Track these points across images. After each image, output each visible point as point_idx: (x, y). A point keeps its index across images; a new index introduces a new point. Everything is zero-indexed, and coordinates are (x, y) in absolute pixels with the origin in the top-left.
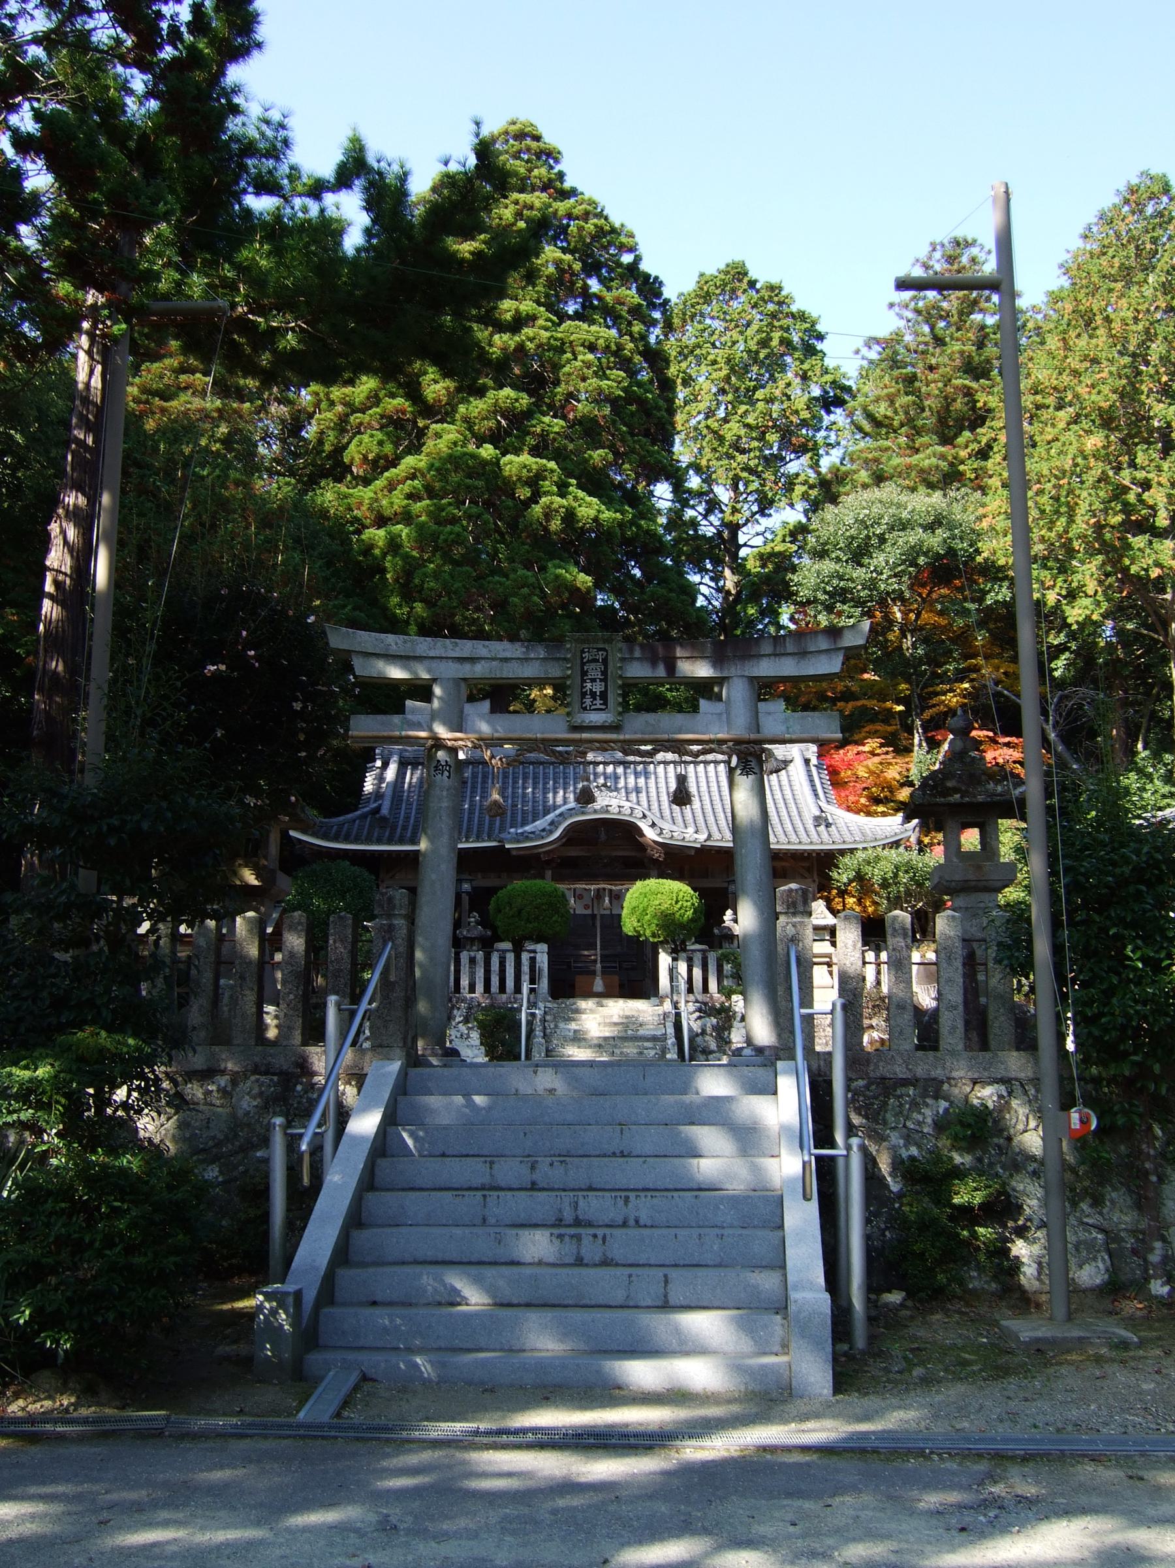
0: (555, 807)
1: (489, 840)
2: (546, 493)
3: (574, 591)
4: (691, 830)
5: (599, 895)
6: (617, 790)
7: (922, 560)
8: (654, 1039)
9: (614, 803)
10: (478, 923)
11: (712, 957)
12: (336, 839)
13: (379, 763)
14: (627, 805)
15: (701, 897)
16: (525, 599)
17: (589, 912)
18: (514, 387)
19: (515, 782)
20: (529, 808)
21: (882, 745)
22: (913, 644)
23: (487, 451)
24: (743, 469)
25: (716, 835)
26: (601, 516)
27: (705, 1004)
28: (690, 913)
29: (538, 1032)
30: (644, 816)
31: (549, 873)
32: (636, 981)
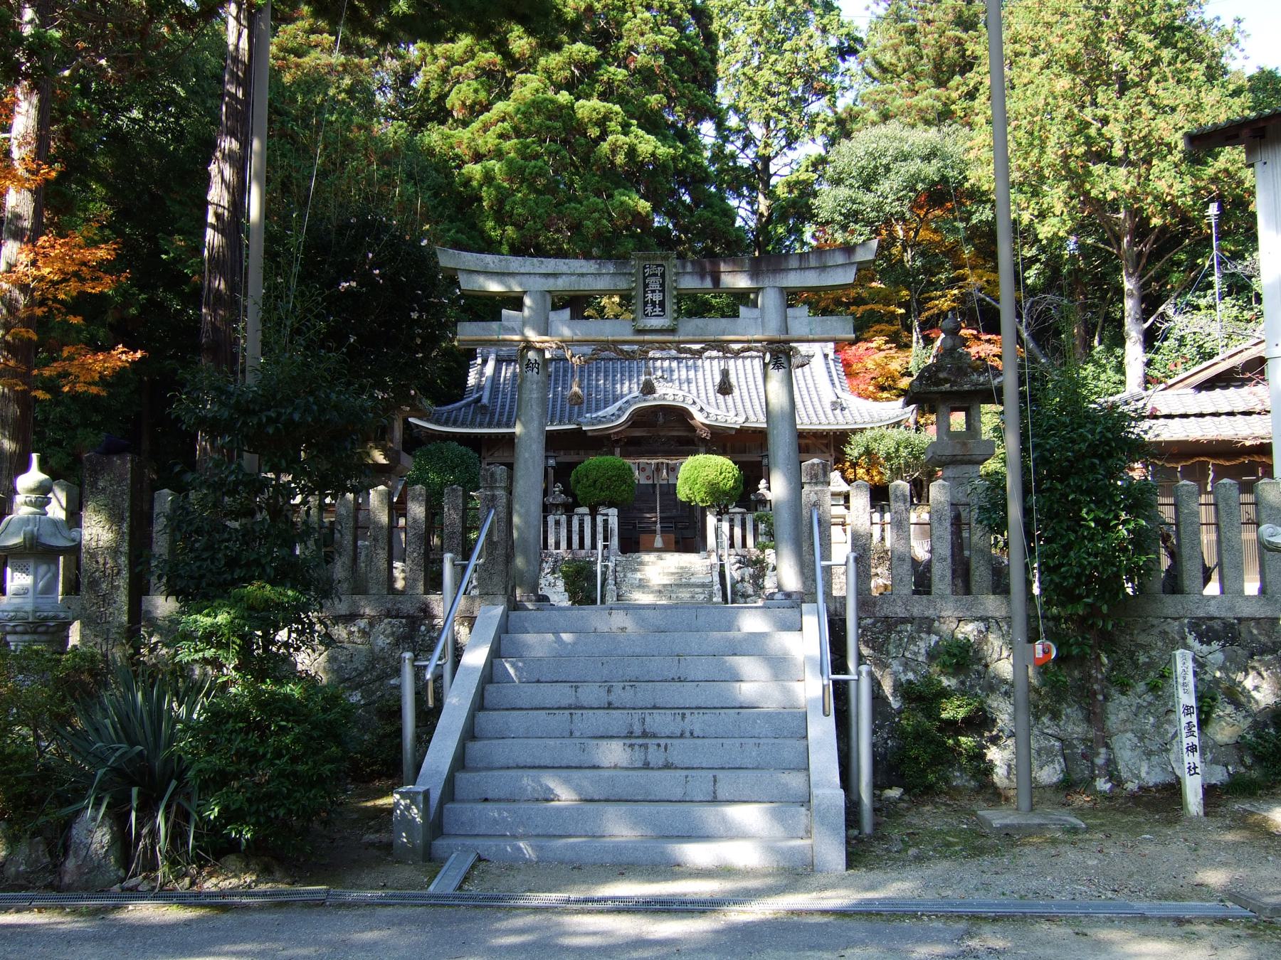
0: (622, 396)
1: (570, 423)
2: (613, 132)
3: (636, 215)
4: (732, 413)
5: (658, 468)
6: (672, 381)
7: (920, 186)
8: (703, 585)
9: (670, 392)
10: (561, 492)
11: (750, 518)
12: (446, 424)
13: (479, 361)
14: (681, 393)
15: (740, 469)
16: (597, 221)
17: (650, 482)
18: (585, 42)
19: (590, 375)
20: (601, 396)
21: (887, 342)
22: (913, 257)
23: (564, 97)
24: (773, 110)
25: (752, 418)
26: (658, 151)
27: (744, 557)
28: (731, 483)
29: (611, 581)
30: (694, 403)
31: (618, 450)
32: (686, 534)
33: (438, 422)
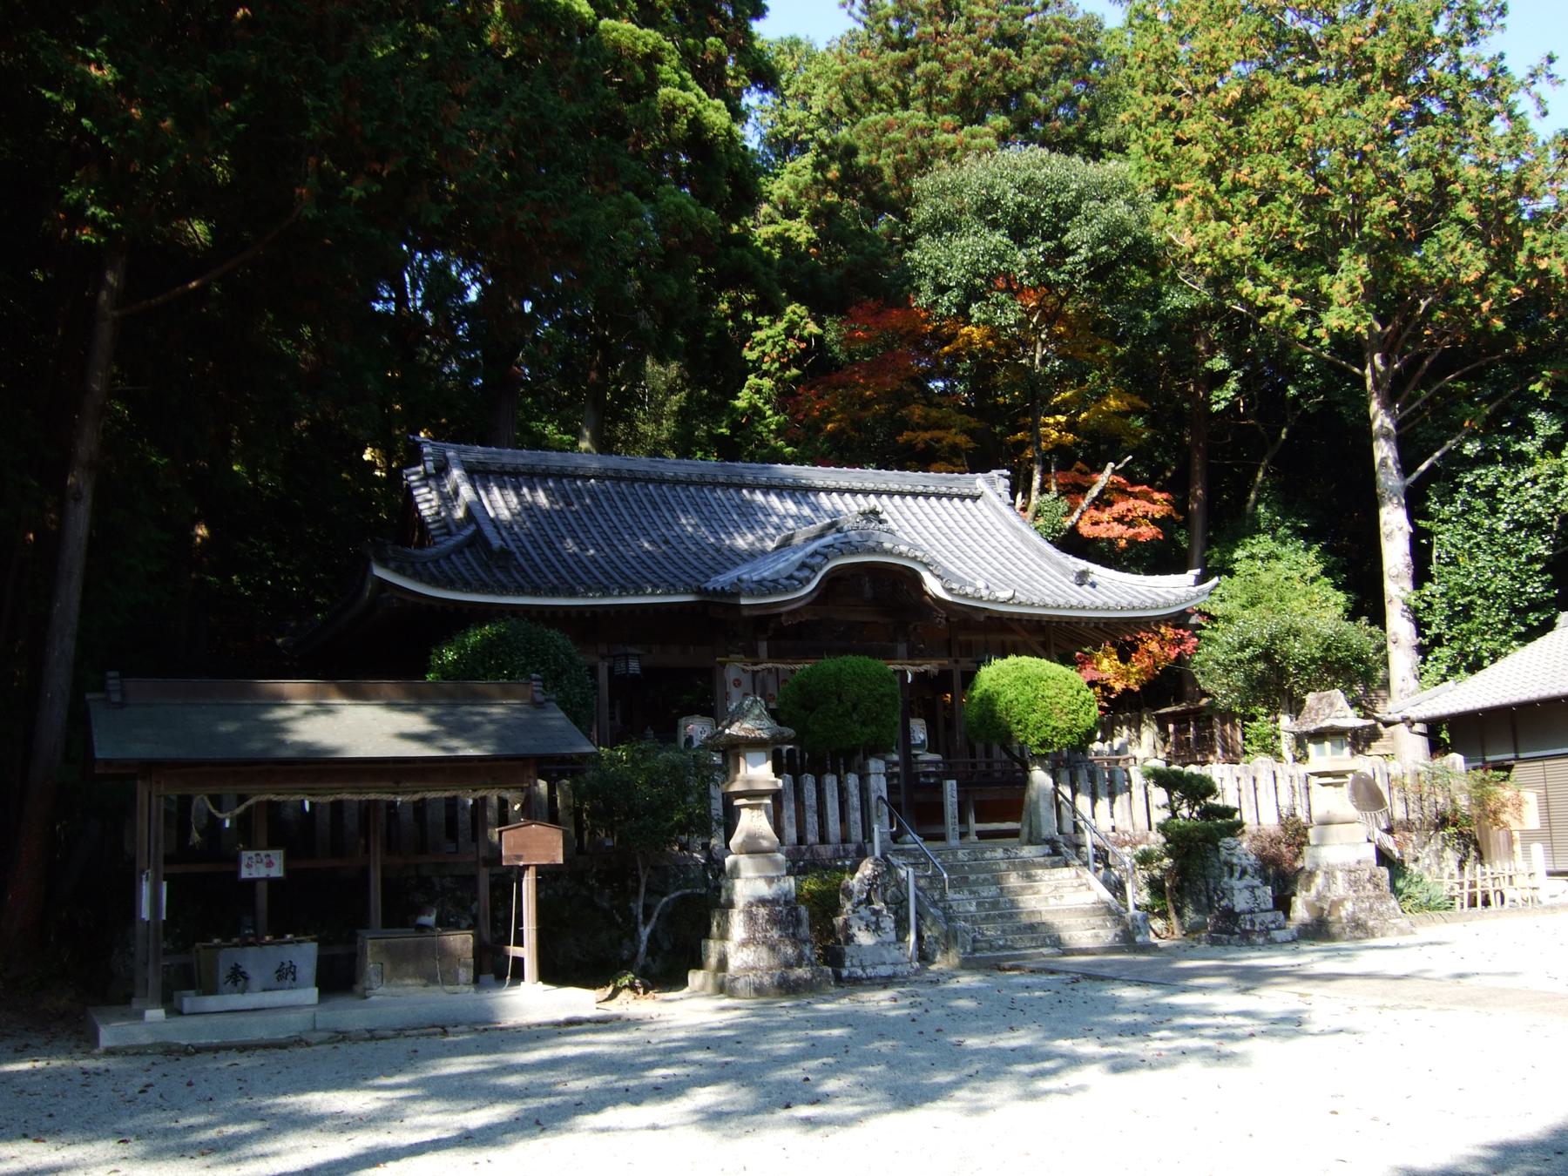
2: (666, 83)
33: (434, 581)
